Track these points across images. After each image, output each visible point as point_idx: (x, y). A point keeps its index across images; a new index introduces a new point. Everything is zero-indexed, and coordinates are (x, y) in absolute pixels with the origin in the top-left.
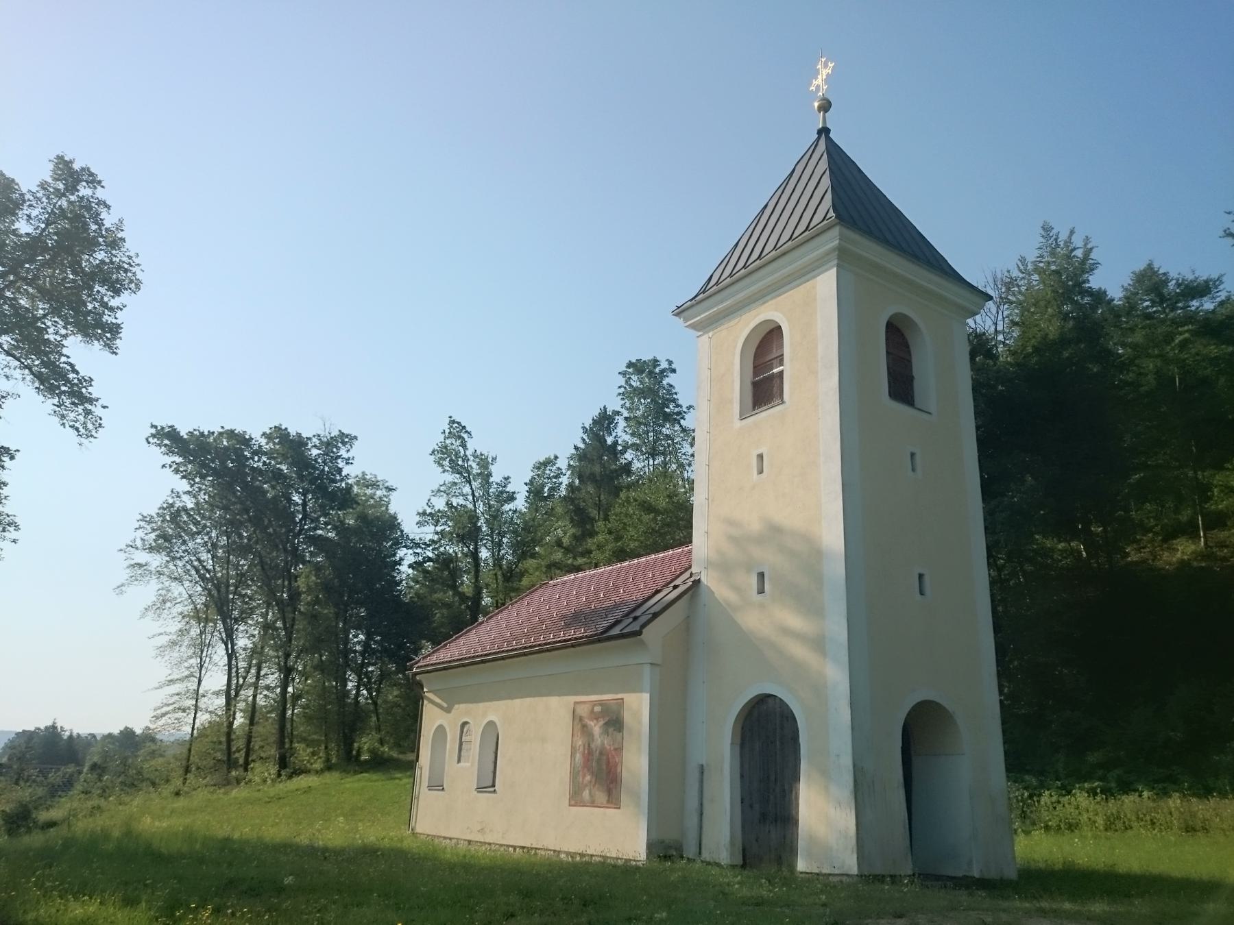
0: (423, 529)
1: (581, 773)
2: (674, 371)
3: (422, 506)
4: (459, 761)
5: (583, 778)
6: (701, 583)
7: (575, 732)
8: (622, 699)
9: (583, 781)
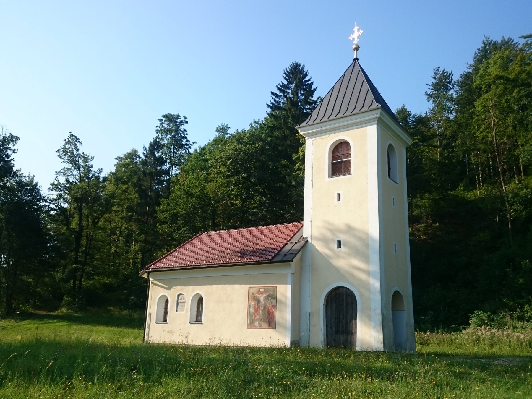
0: (51, 192)
1: (253, 315)
2: (187, 122)
3: (53, 180)
4: (177, 311)
5: (255, 318)
6: (308, 242)
7: (249, 299)
8: (276, 286)
9: (255, 319)
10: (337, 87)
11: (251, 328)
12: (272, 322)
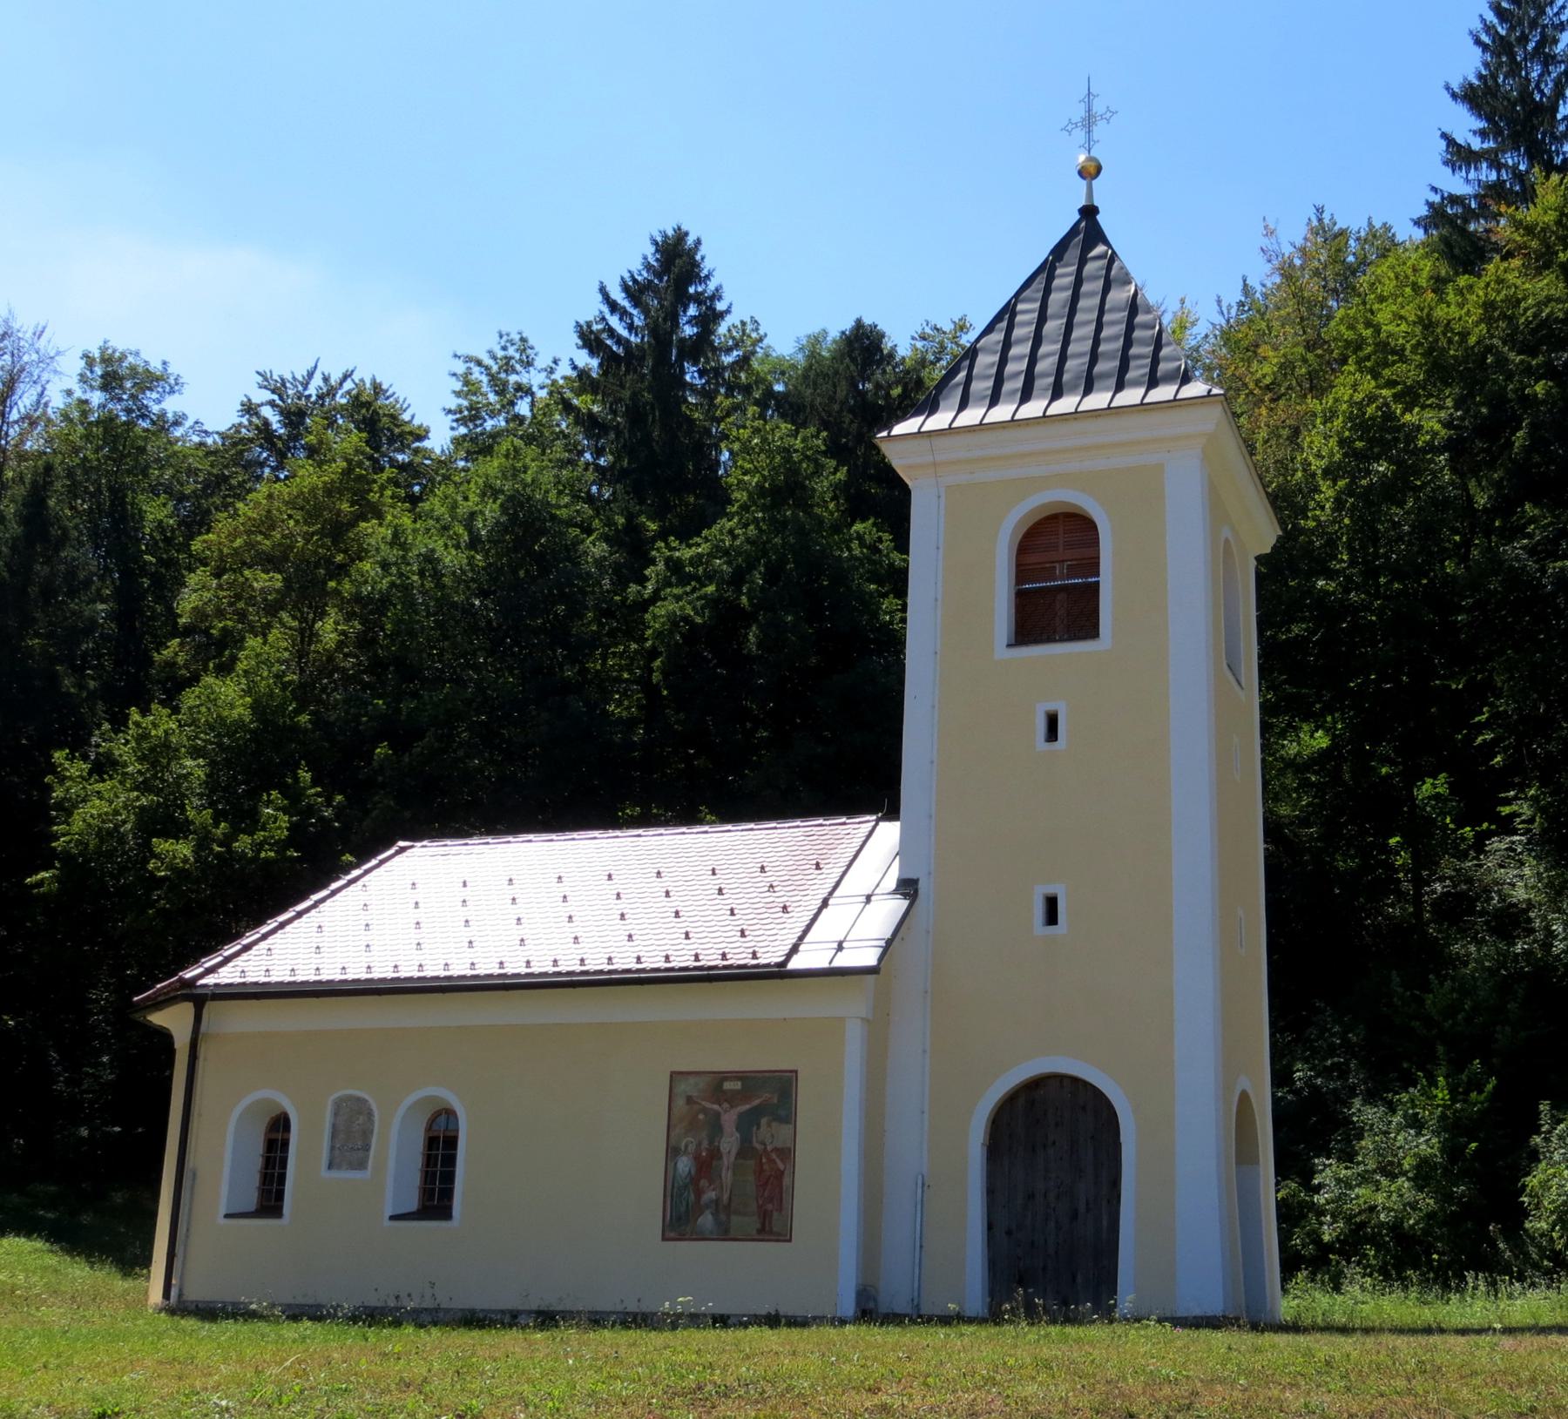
10: (1028, 311)
11: (681, 1238)
12: (775, 1214)
